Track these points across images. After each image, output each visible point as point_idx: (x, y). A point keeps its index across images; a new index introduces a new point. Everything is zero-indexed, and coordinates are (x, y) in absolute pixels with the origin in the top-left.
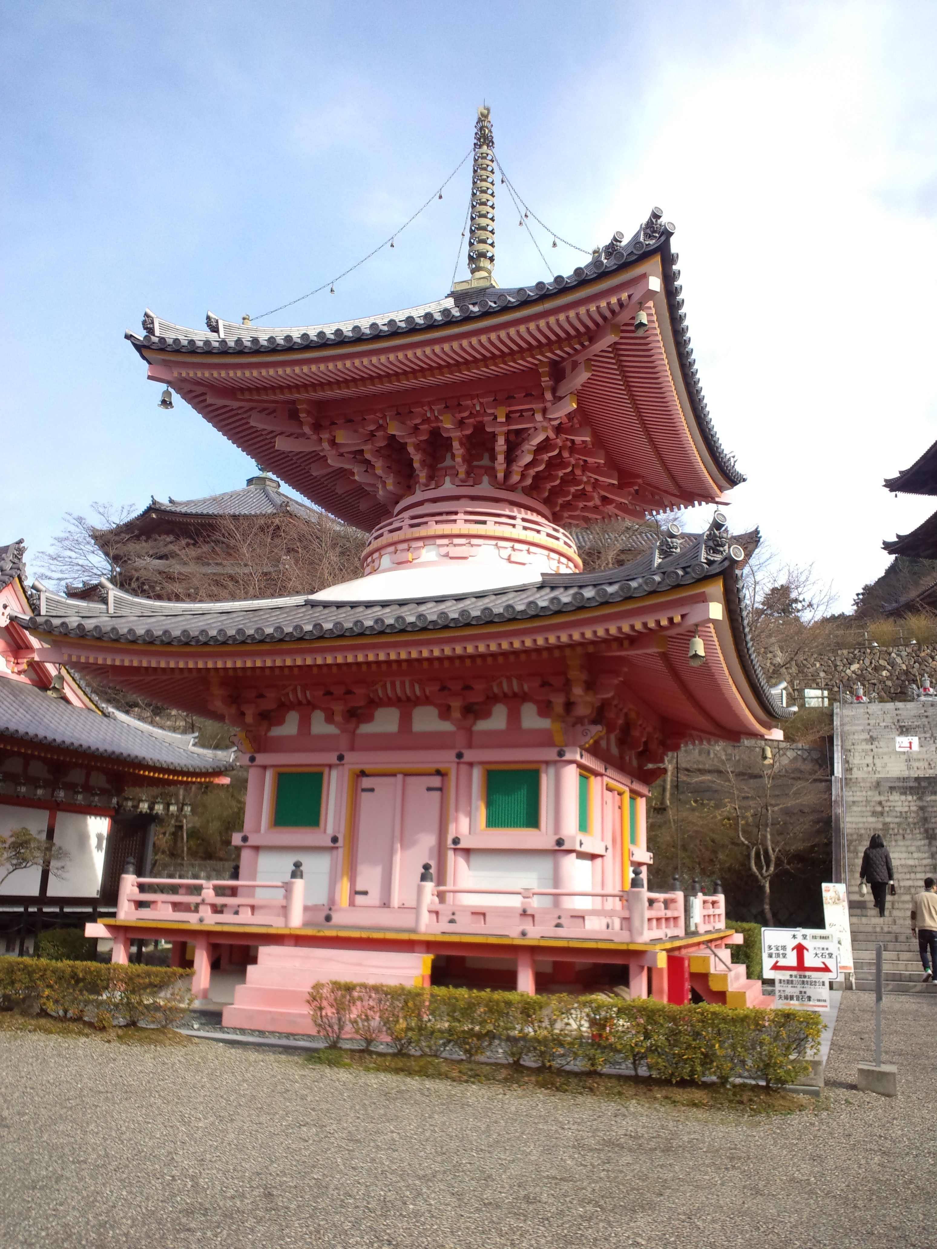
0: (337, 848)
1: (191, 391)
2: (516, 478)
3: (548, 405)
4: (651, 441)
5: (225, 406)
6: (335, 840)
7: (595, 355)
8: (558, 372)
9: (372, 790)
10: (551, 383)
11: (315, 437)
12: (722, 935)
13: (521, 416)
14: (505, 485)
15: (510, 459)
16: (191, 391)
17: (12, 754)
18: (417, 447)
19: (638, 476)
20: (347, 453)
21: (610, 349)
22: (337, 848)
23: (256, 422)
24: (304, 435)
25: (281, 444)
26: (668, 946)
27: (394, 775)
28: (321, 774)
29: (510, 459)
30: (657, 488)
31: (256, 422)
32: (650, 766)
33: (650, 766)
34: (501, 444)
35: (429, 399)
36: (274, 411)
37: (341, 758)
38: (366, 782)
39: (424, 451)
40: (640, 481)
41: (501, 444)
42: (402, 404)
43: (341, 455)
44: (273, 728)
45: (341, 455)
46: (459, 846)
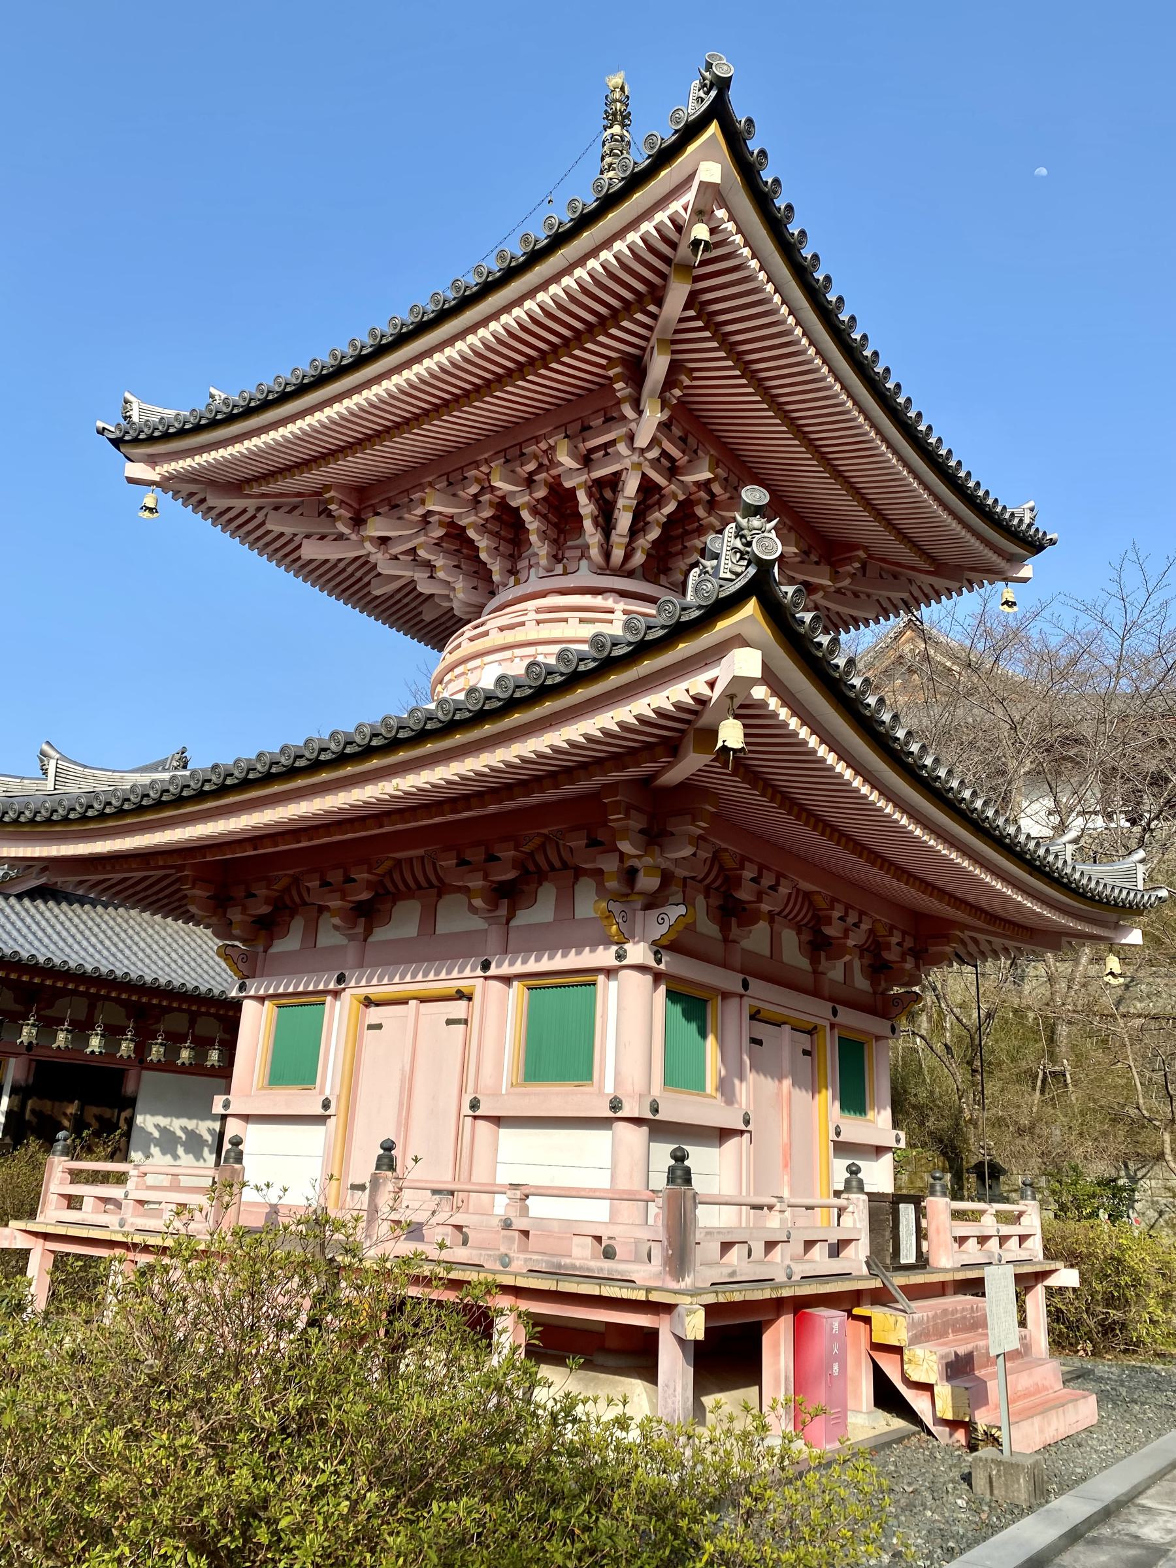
0: (329, 1116)
1: (191, 495)
2: (618, 554)
3: (633, 426)
4: (837, 474)
5: (229, 509)
6: (326, 1105)
7: (677, 331)
8: (636, 369)
9: (379, 1027)
10: (629, 390)
11: (354, 537)
12: (1038, 1269)
13: (607, 454)
14: (606, 569)
15: (606, 522)
16: (191, 495)
17: (64, 992)
18: (483, 528)
19: (855, 546)
20: (403, 553)
21: (692, 313)
22: (329, 1116)
23: (275, 525)
24: (340, 537)
25: (311, 551)
26: (710, 1299)
27: (404, 1002)
28: (861, 1045)
29: (606, 522)
30: (899, 565)
31: (275, 525)
32: (896, 990)
33: (896, 990)
34: (586, 506)
35: (486, 456)
36: (295, 508)
37: (341, 979)
38: (375, 1015)
39: (496, 535)
40: (862, 554)
41: (586, 506)
42: (450, 467)
43: (396, 558)
44: (276, 942)
45: (396, 558)
46: (478, 1113)
